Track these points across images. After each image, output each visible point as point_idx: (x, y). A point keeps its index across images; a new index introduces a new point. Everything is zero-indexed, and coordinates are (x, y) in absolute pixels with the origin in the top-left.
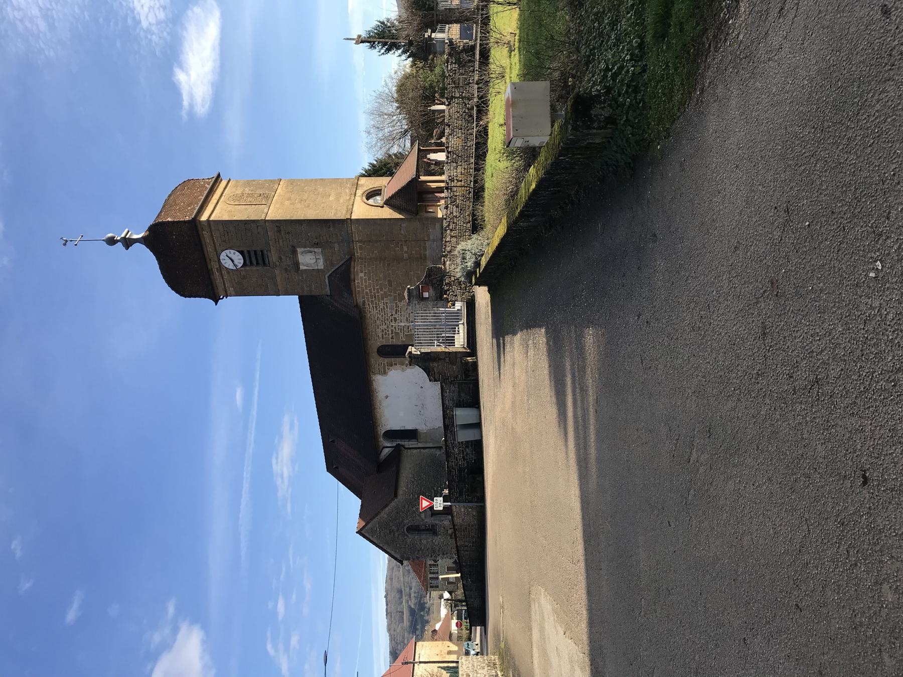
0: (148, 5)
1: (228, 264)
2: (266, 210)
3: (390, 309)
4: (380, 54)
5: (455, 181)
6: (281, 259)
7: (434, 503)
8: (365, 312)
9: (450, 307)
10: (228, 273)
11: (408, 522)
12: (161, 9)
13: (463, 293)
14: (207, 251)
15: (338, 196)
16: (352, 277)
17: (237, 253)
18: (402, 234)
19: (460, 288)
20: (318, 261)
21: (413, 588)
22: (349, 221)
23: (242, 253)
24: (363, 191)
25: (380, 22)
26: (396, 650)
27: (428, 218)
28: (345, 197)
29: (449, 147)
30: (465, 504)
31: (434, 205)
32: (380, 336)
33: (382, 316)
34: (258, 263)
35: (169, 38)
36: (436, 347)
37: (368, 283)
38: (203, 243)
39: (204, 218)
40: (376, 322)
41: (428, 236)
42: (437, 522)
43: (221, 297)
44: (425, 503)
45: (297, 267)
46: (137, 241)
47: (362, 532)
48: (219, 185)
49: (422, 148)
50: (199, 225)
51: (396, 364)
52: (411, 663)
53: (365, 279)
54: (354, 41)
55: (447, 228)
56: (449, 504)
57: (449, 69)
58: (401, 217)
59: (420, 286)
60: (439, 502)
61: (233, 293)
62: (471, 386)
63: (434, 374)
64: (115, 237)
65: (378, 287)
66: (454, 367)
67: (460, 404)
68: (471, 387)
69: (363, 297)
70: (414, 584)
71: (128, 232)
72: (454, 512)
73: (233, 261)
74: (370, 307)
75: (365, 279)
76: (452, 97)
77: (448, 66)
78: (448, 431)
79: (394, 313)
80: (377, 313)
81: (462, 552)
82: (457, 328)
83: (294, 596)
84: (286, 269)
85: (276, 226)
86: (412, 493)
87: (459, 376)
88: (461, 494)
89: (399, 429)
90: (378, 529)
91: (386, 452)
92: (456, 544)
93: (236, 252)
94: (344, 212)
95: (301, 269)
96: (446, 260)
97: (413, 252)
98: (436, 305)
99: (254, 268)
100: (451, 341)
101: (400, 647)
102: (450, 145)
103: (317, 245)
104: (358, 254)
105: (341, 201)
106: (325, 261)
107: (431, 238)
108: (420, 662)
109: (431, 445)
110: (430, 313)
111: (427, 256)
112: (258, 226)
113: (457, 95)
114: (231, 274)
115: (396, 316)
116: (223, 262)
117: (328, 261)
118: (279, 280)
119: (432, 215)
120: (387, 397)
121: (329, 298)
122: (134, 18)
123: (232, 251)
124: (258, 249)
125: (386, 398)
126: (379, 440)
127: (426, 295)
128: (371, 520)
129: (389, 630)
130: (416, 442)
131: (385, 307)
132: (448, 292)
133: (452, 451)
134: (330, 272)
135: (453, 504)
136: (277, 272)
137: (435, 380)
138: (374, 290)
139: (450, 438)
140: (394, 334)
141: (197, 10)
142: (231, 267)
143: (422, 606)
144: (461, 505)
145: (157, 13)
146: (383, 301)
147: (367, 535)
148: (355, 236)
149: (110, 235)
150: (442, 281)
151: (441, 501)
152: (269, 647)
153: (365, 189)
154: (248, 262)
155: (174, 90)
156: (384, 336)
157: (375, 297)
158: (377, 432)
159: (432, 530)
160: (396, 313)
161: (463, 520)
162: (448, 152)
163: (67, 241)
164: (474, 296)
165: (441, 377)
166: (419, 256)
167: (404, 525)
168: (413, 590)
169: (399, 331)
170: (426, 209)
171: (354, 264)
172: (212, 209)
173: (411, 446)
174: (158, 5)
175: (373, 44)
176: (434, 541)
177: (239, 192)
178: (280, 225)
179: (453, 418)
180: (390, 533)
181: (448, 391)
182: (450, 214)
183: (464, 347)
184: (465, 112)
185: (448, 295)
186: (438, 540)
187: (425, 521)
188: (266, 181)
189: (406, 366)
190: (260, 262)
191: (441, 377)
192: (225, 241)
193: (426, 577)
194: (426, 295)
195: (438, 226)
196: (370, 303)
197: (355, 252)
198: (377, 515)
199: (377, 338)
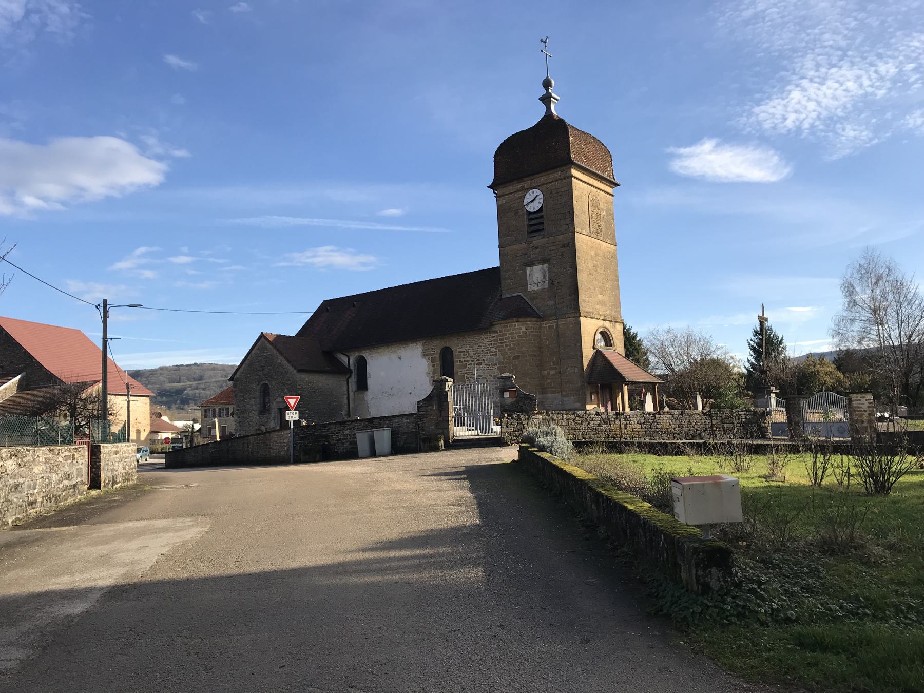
1: (528, 197)
2: (584, 232)
4: (749, 341)
5: (625, 423)
6: (536, 248)
7: (292, 411)
8: (486, 333)
9: (494, 420)
10: (520, 198)
11: (273, 385)
12: (773, 125)
13: (510, 434)
14: (542, 176)
15: (602, 303)
16: (520, 320)
17: (540, 206)
19: (515, 430)
20: (536, 285)
21: (204, 392)
22: (578, 315)
23: (541, 210)
24: (609, 328)
25: (782, 339)
26: (141, 376)
27: (585, 395)
28: (602, 310)
29: (660, 415)
30: (291, 444)
31: (598, 401)
32: (462, 350)
33: (482, 351)
34: (531, 226)
36: (454, 406)
39: (574, 172)
40: (476, 344)
41: (567, 396)
42: (273, 415)
43: (496, 192)
44: (292, 402)
45: (529, 265)
46: (549, 108)
47: (263, 339)
48: (607, 185)
49: (656, 386)
51: (434, 366)
52: (128, 392)
53: (519, 333)
54: (761, 315)
55: (576, 415)
56: (292, 427)
57: (740, 413)
58: (585, 367)
59: (516, 389)
60: (293, 416)
61: (500, 203)
62: (414, 445)
63: (426, 406)
64: (551, 87)
65: (512, 346)
66: (433, 427)
67: (395, 435)
68: (412, 445)
69: (501, 331)
70: (208, 392)
71: (557, 100)
72: (284, 432)
73: (532, 201)
74: (492, 337)
76: (710, 416)
77: (743, 411)
78: (367, 423)
79: (486, 362)
80: (486, 346)
81: (242, 442)
82: (474, 428)
83: (192, 272)
84: (526, 254)
85: (569, 243)
86: (302, 388)
87: (424, 432)
88: (302, 438)
89: (368, 372)
90: (265, 354)
91: (344, 359)
92: (251, 435)
93: (541, 205)
94: (587, 309)
95: (527, 268)
96: (544, 414)
98: (497, 406)
99: (526, 223)
100: (459, 422)
101: (144, 381)
102: (661, 416)
103: (552, 283)
104: (545, 325)
105: (598, 307)
106: (536, 292)
107: (565, 399)
108: (129, 402)
109: (351, 405)
110: (488, 399)
113: (714, 422)
114: (519, 201)
116: (531, 192)
117: (535, 296)
118: (514, 247)
120: (400, 358)
121: (498, 297)
122: (762, 100)
123: (542, 201)
124: (545, 226)
125: (399, 358)
126: (356, 352)
127: (507, 395)
128: (275, 347)
129: (162, 368)
130: (354, 390)
132: (510, 418)
133: (346, 428)
135: (292, 431)
136: (523, 245)
137: (419, 408)
139: (360, 425)
140: (464, 363)
141: (775, 159)
143: (185, 401)
144: (291, 439)
145: (768, 121)
147: (259, 343)
148: (562, 321)
149: (553, 82)
150: (522, 411)
151: (295, 418)
152: (142, 250)
153: (611, 330)
154: (531, 216)
155: (694, 139)
156: (462, 353)
157: (501, 343)
158: (365, 350)
159: (264, 409)
161: (276, 442)
162: (654, 414)
163: (545, 42)
164: (508, 445)
165: (422, 413)
167: (269, 381)
168: (202, 391)
169: (467, 368)
170: (594, 392)
172: (583, 180)
173: (350, 384)
174: (776, 121)
175: (759, 334)
176: (253, 412)
177: (601, 205)
178: (571, 245)
179: (380, 428)
180: (262, 367)
181: (408, 421)
182: (591, 418)
183: (454, 436)
184: (697, 430)
185: (507, 418)
186: (254, 416)
187: (274, 402)
188: (614, 231)
189: (432, 377)
190: (533, 228)
191: (422, 413)
192: (551, 193)
193: (216, 404)
194: (507, 395)
195: (578, 405)
196: (494, 338)
198: (280, 352)
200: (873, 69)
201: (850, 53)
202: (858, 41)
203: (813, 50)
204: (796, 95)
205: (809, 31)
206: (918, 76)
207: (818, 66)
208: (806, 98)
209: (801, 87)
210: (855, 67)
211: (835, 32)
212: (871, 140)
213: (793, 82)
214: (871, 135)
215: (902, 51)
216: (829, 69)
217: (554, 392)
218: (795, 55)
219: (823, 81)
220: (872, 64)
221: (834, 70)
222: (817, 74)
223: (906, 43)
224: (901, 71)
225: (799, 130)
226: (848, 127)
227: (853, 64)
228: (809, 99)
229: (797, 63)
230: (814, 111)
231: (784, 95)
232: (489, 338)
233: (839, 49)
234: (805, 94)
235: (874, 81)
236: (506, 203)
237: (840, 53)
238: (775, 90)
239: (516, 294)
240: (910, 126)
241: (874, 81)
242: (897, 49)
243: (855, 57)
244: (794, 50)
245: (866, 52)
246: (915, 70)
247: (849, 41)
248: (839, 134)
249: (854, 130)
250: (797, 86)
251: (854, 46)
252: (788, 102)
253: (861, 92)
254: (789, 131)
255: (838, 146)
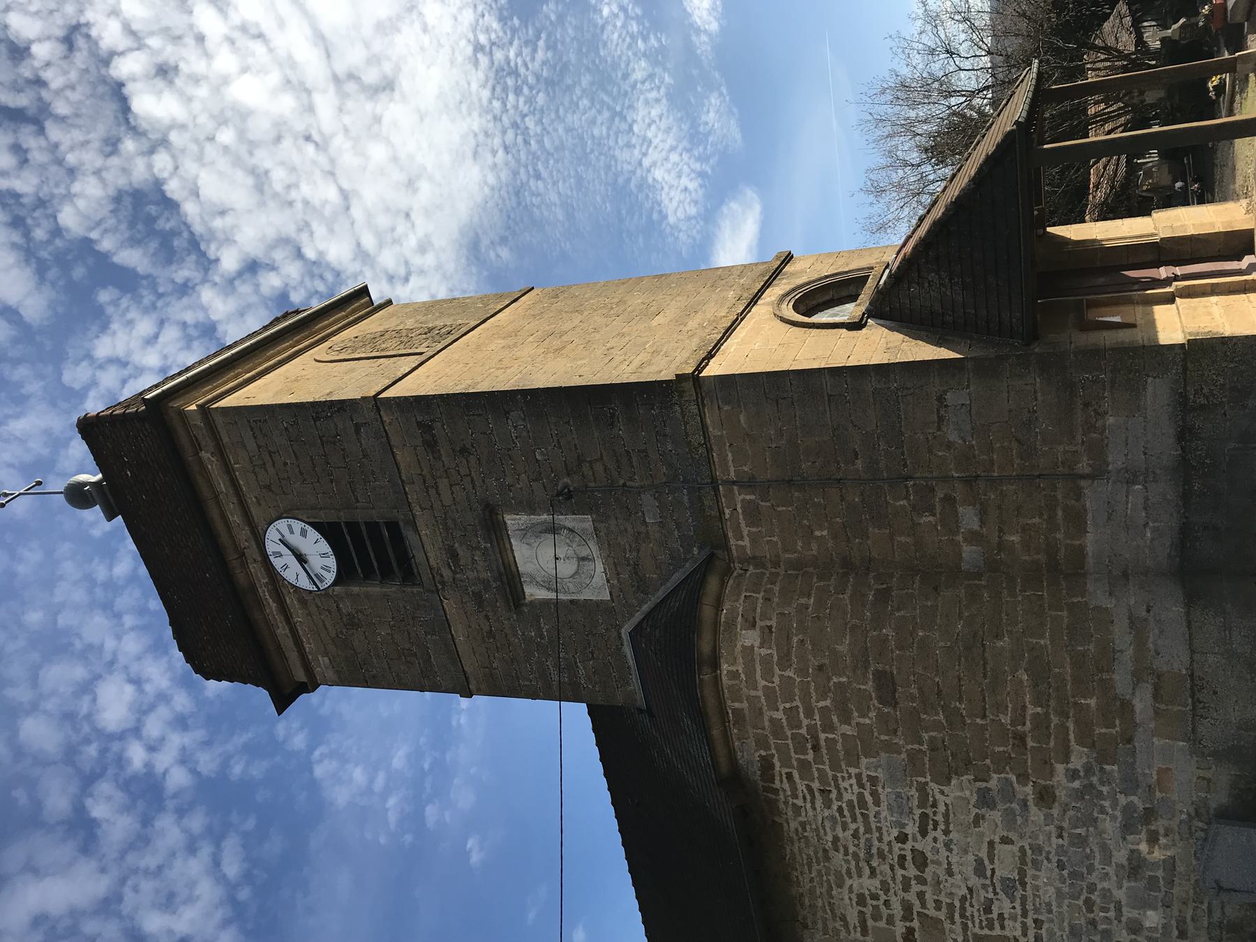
0: (677, 199)
1: (292, 572)
3: (890, 808)
6: (454, 555)
8: (773, 804)
12: (692, 204)
17: (313, 534)
18: (949, 446)
20: (588, 566)
22: (688, 386)
23: (328, 531)
24: (788, 288)
27: (1096, 353)
32: (853, 918)
33: (855, 835)
35: (698, 237)
37: (776, 680)
38: (206, 492)
40: (827, 859)
50: (181, 431)
53: (766, 661)
61: (330, 674)
65: (828, 703)
69: (762, 743)
74: (794, 788)
75: (766, 661)
79: (911, 829)
84: (478, 598)
85: (419, 424)
93: (309, 529)
95: (528, 599)
97: (1015, 538)
103: (566, 499)
104: (742, 541)
106: (614, 566)
107: (1116, 460)
111: (1090, 561)
112: (357, 428)
115: (924, 845)
118: (460, 639)
119: (1124, 336)
122: (660, 212)
123: (297, 525)
131: (869, 798)
134: (638, 617)
138: (809, 713)
140: (916, 924)
141: (734, 205)
142: (304, 583)
145: (687, 209)
146: (853, 771)
156: (870, 923)
157: (816, 748)
160: (924, 833)
166: (1042, 557)
169: (942, 915)
171: (723, 584)
174: (688, 200)
192: (268, 487)
197: (730, 534)
199: (838, 924)
200: (639, 86)
201: (618, 109)
202: (606, 98)
203: (610, 148)
204: (658, 174)
205: (588, 150)
206: (652, 36)
207: (629, 146)
208: (665, 162)
209: (651, 167)
210: (635, 104)
211: (593, 122)
212: (721, 94)
213: (644, 175)
214: (716, 94)
215: (622, 51)
216: (633, 134)
217: (1077, 521)
218: (613, 168)
219: (647, 142)
220: (634, 86)
221: (636, 128)
222: (638, 147)
223: (613, 47)
224: (644, 55)
225: (702, 175)
226: (704, 118)
227: (631, 107)
228: (666, 159)
229: (622, 168)
230: (681, 155)
231: (658, 186)
232: (796, 797)
233: (612, 119)
234: (659, 164)
235: (653, 85)
236: (326, 654)
237: (617, 120)
238: (651, 195)
239: (628, 650)
240: (709, 49)
241: (653, 85)
242: (620, 57)
243: (624, 104)
244: (608, 167)
245: (619, 91)
246: (645, 39)
247: (605, 107)
248: (711, 129)
249: (709, 112)
250: (649, 171)
251: (611, 103)
252: (666, 183)
253: (664, 101)
254: (701, 186)
255: (725, 131)
